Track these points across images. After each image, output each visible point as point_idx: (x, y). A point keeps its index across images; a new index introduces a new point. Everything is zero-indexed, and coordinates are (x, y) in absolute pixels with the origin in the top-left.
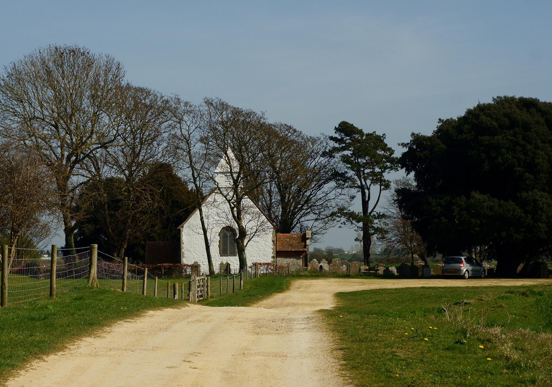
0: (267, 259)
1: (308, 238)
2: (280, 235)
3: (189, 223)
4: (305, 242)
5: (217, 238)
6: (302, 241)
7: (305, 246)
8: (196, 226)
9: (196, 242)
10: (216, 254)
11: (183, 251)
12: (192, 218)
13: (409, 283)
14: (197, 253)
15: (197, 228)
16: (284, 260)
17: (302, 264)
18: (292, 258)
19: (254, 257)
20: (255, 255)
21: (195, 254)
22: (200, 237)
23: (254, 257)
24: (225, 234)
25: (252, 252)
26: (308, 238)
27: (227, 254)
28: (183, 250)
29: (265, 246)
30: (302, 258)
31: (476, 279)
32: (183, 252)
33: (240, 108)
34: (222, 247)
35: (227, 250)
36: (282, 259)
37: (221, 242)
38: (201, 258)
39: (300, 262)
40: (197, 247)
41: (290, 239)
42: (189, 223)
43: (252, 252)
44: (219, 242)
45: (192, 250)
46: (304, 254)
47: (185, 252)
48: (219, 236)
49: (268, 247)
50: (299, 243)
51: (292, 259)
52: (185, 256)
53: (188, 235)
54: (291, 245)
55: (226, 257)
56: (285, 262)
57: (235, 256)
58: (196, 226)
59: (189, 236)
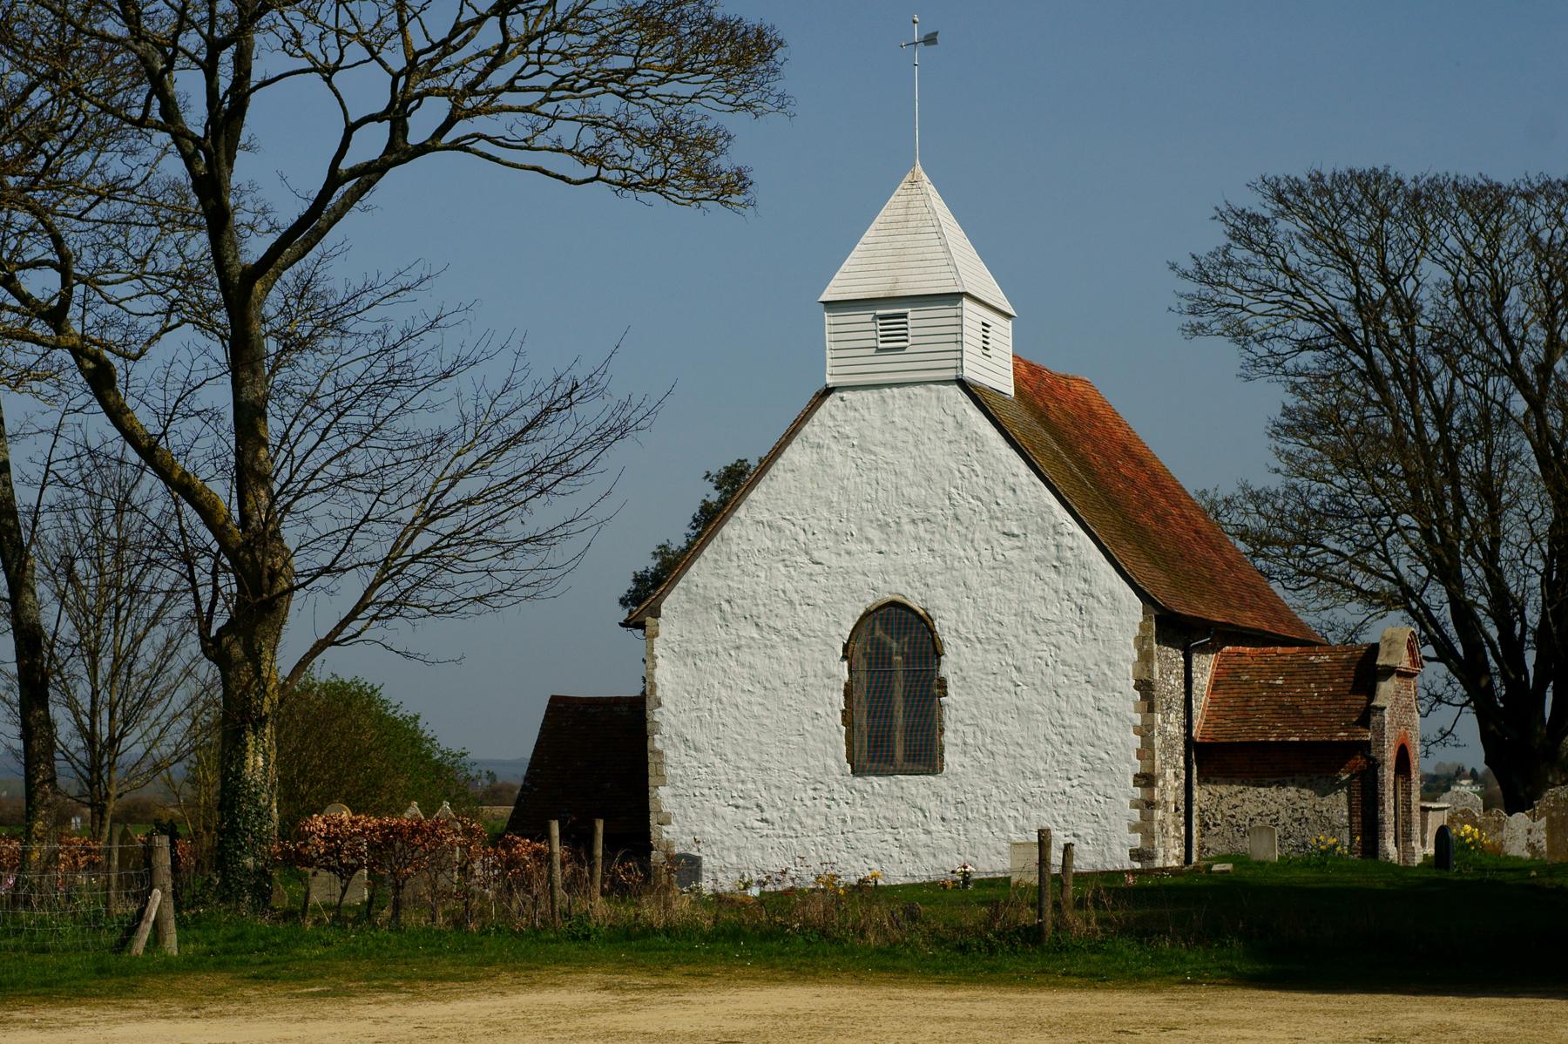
0: (1110, 792)
1: (1389, 671)
2: (1240, 654)
3: (687, 591)
4: (1371, 693)
5: (835, 670)
6: (1356, 690)
7: (1367, 715)
8: (725, 606)
9: (724, 693)
10: (831, 763)
11: (658, 745)
12: (701, 560)
13: (495, 1011)
14: (731, 757)
15: (729, 617)
16: (1247, 795)
17: (1350, 817)
18: (1293, 783)
19: (1037, 776)
20: (1041, 766)
21: (717, 761)
22: (743, 665)
23: (1037, 776)
24: (878, 646)
25: (1028, 752)
26: (1389, 671)
27: (890, 759)
28: (657, 742)
29: (1097, 716)
30: (1348, 783)
31: (956, 983)
32: (660, 753)
33: (1441, 173)
34: (862, 720)
35: (889, 736)
36: (1236, 788)
37: (861, 694)
38: (750, 786)
39: (1338, 806)
40: (729, 721)
41: (1290, 675)
42: (687, 591)
43: (1028, 752)
44: (848, 693)
45: (701, 738)
46: (1359, 761)
47: (670, 753)
48: (845, 657)
49: (1114, 721)
50: (1335, 697)
51: (1291, 792)
52: (669, 771)
53: (686, 655)
54: (1292, 712)
55: (884, 781)
56: (1251, 809)
57: (934, 773)
58: (725, 606)
59: (689, 661)
